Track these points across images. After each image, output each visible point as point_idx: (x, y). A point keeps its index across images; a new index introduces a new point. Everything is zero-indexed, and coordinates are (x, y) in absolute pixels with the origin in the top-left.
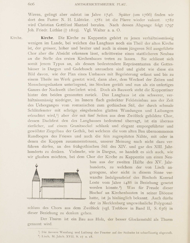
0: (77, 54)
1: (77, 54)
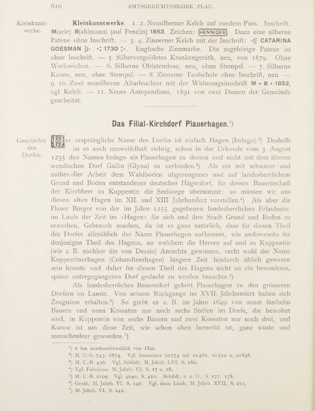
0: (196, 50)
1: (196, 50)
